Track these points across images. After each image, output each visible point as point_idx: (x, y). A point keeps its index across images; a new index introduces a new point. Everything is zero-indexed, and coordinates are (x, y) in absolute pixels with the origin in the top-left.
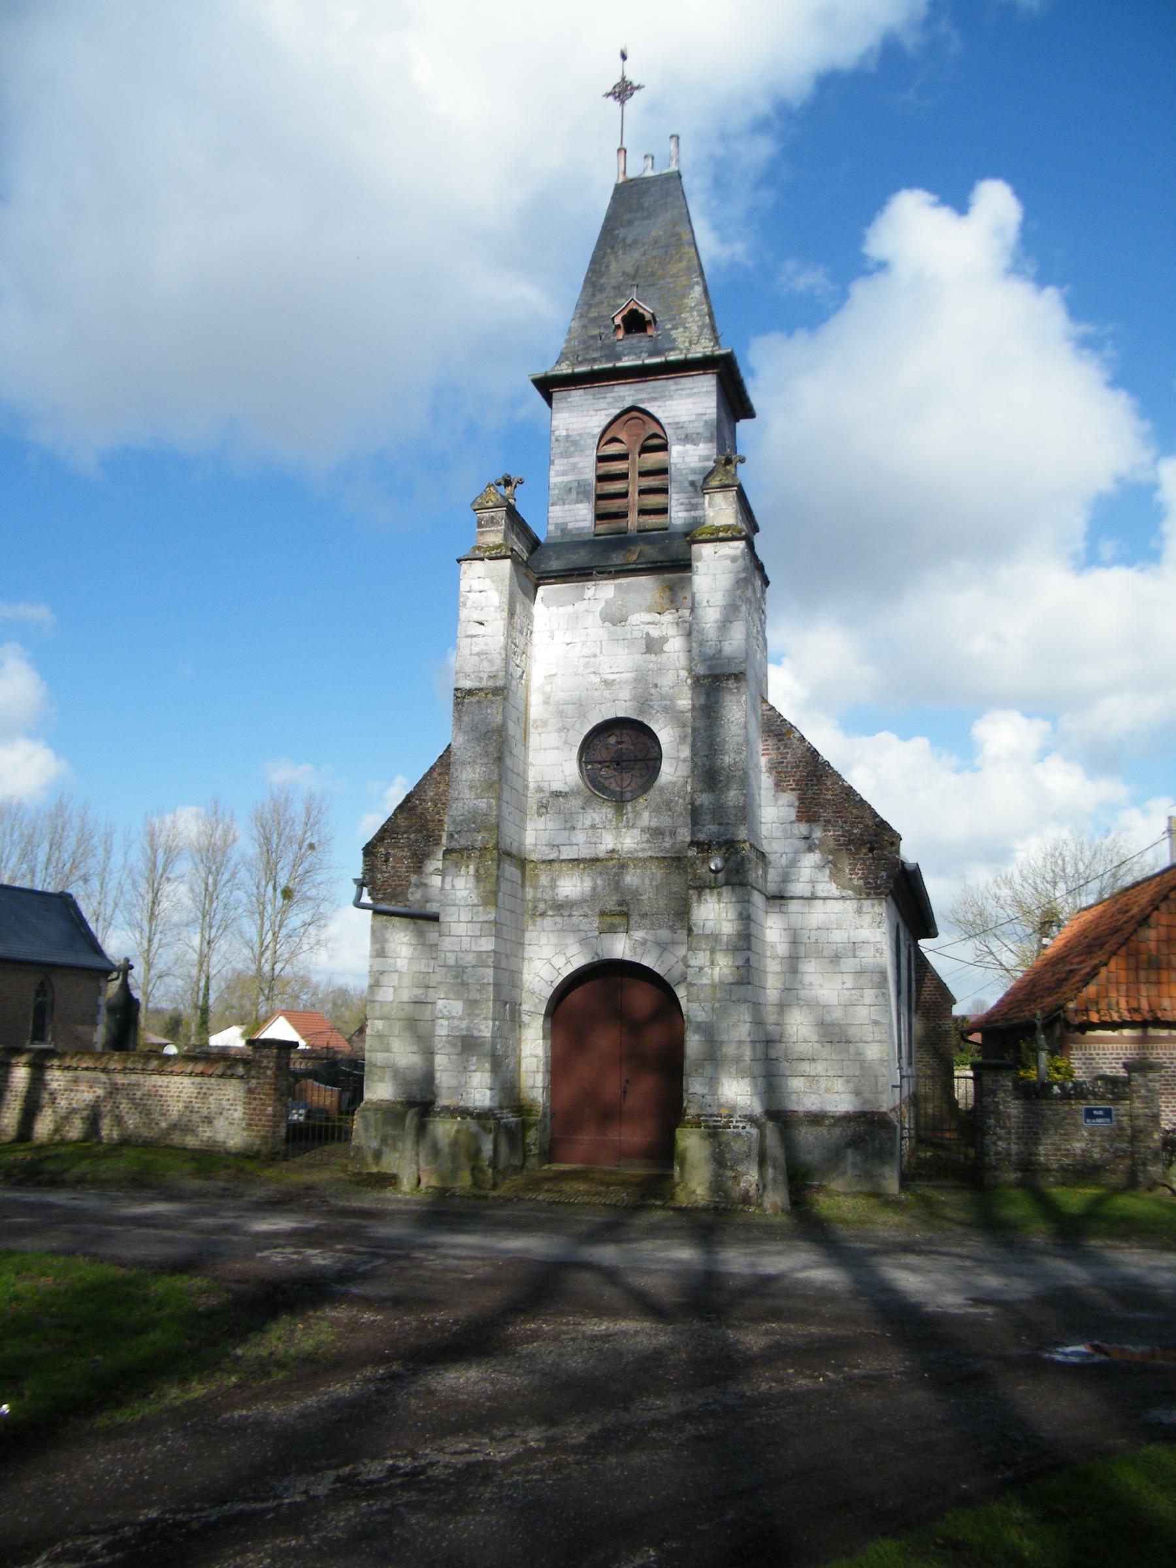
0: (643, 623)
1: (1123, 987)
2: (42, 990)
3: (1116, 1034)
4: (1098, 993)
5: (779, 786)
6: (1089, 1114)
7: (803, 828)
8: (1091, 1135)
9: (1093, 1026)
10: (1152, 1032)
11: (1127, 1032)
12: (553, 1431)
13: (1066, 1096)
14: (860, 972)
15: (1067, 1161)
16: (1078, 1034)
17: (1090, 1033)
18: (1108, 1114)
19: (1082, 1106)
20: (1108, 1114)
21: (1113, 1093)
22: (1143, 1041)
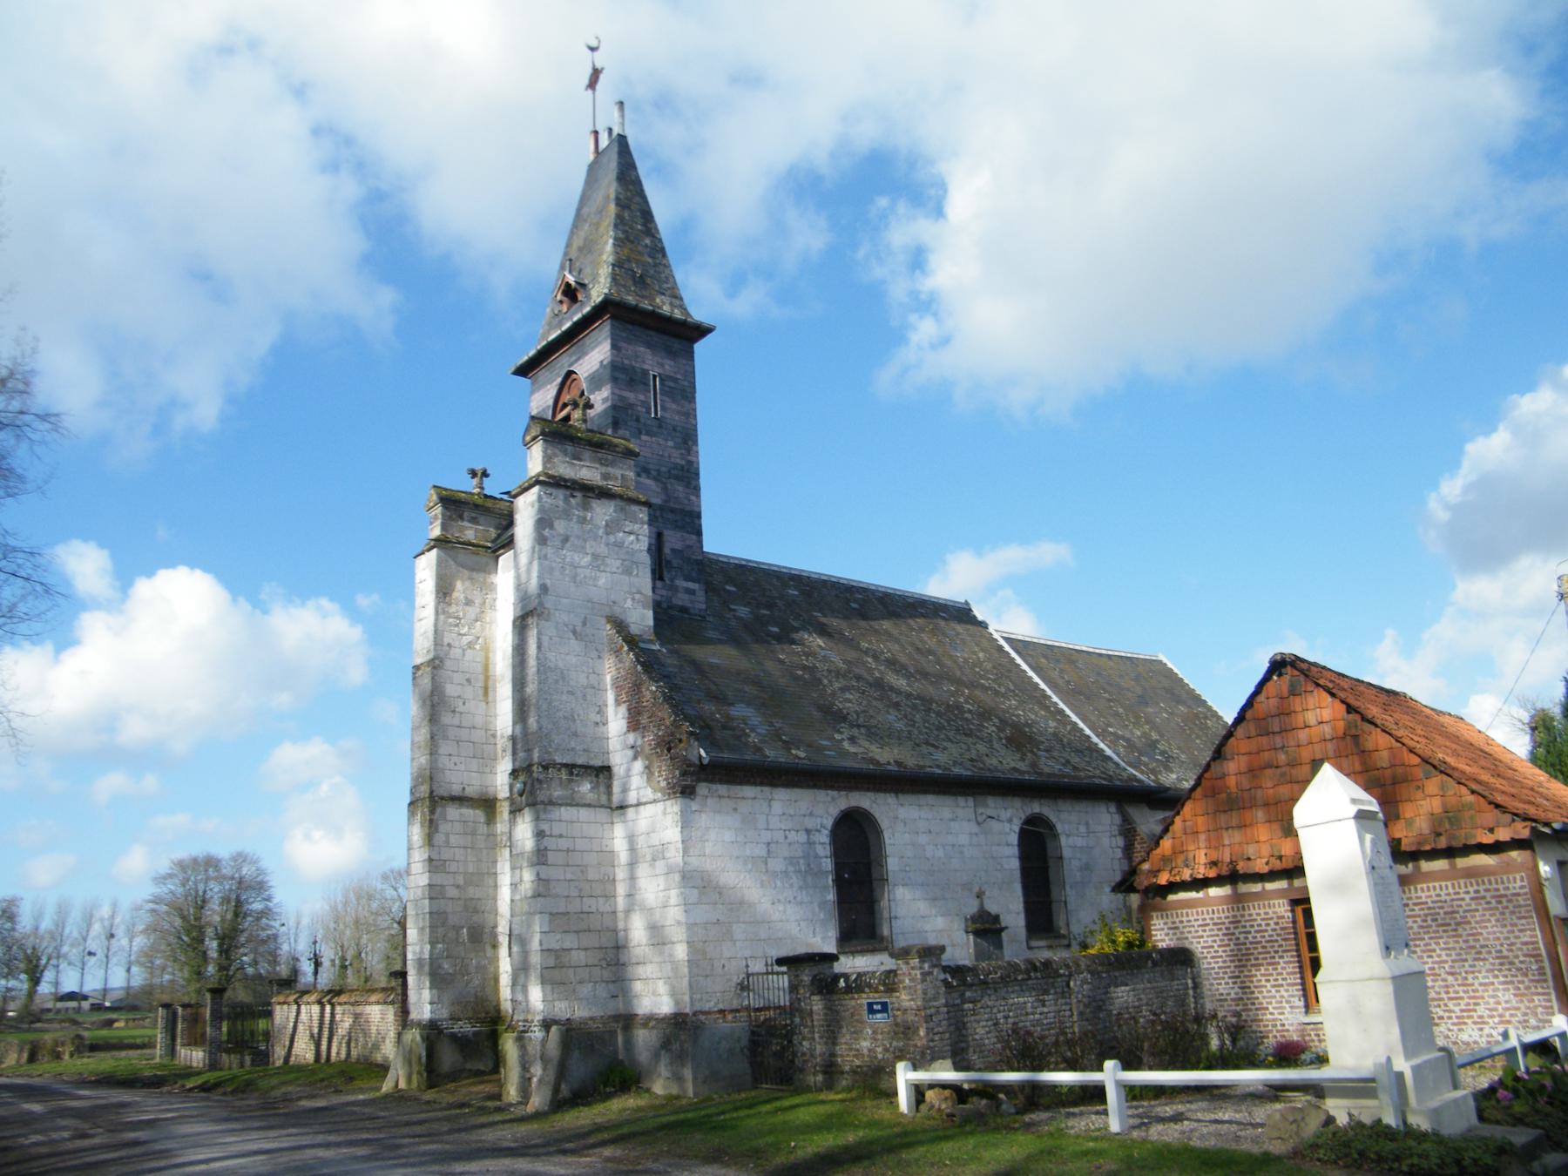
0: (83, 1083)
1: (1202, 837)
2: (1463, 1066)
3: (1201, 895)
4: (1173, 847)
5: (618, 703)
6: (871, 1011)
7: (631, 738)
8: (874, 1032)
9: (1173, 887)
10: (1245, 888)
11: (1214, 891)
12: (630, 396)
13: (848, 990)
14: (78, 1036)
15: (858, 1063)
16: (1158, 899)
17: (1171, 897)
18: (885, 1008)
19: (863, 1000)
20: (885, 1008)
21: (884, 984)
22: (1238, 900)
